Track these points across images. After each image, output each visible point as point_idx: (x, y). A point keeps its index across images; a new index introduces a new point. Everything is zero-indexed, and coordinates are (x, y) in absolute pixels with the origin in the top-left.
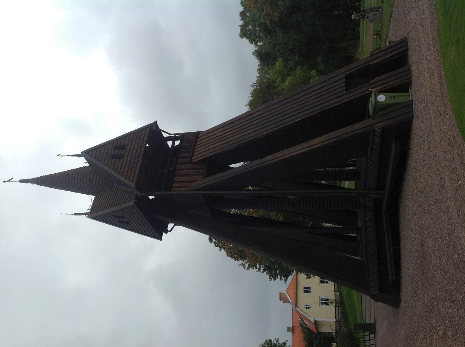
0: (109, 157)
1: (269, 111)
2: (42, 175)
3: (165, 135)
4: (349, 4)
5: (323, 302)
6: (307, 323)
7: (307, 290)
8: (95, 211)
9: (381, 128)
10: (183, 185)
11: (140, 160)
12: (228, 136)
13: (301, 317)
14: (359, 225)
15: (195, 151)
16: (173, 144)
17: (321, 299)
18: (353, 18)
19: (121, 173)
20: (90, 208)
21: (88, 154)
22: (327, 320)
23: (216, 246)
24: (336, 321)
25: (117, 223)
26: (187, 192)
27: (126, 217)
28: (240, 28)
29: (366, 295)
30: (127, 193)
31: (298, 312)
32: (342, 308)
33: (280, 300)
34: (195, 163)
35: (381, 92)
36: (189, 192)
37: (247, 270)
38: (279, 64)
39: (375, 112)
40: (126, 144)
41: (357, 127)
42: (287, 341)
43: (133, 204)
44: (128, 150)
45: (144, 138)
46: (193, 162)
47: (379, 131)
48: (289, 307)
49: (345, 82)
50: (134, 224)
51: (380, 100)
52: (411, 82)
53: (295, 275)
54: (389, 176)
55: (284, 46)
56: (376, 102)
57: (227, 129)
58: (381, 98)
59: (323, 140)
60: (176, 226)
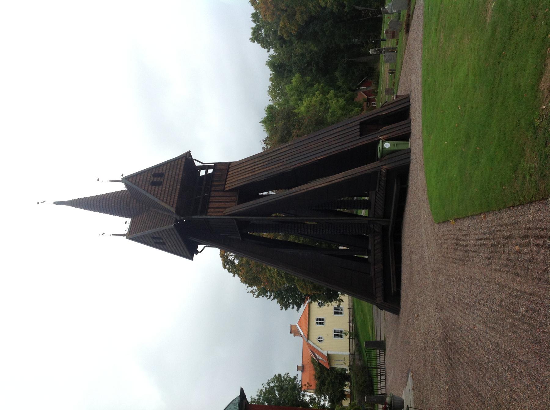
0: (149, 184)
1: (295, 148)
2: (77, 198)
3: (197, 164)
4: (371, 16)
5: (337, 334)
6: (318, 357)
7: (320, 321)
8: (138, 231)
9: (385, 170)
10: (217, 210)
11: (178, 187)
12: (257, 165)
13: (314, 351)
14: (370, 247)
15: (227, 180)
16: (207, 172)
17: (335, 331)
18: (370, 53)
19: (162, 199)
20: (127, 230)
21: (128, 180)
22: (340, 353)
23: (230, 272)
24: (350, 354)
25: (153, 243)
26: (221, 217)
27: (163, 238)
28: (252, 31)
29: (373, 304)
30: (166, 217)
31: (310, 345)
32: (356, 340)
33: (291, 333)
34: (227, 191)
35: (387, 140)
36: (223, 217)
37: (256, 298)
38: (295, 79)
39: (382, 156)
40: (164, 172)
41: (367, 168)
42: (297, 375)
43: (174, 227)
44: (166, 177)
45: (180, 167)
46: (226, 190)
47: (385, 172)
48: (299, 340)
49: (360, 132)
50: (170, 244)
51: (387, 147)
52: (410, 133)
53: (308, 306)
54: (393, 206)
55: (300, 58)
56: (382, 149)
57: (257, 162)
58: (387, 145)
59: (341, 177)
60: (206, 248)
